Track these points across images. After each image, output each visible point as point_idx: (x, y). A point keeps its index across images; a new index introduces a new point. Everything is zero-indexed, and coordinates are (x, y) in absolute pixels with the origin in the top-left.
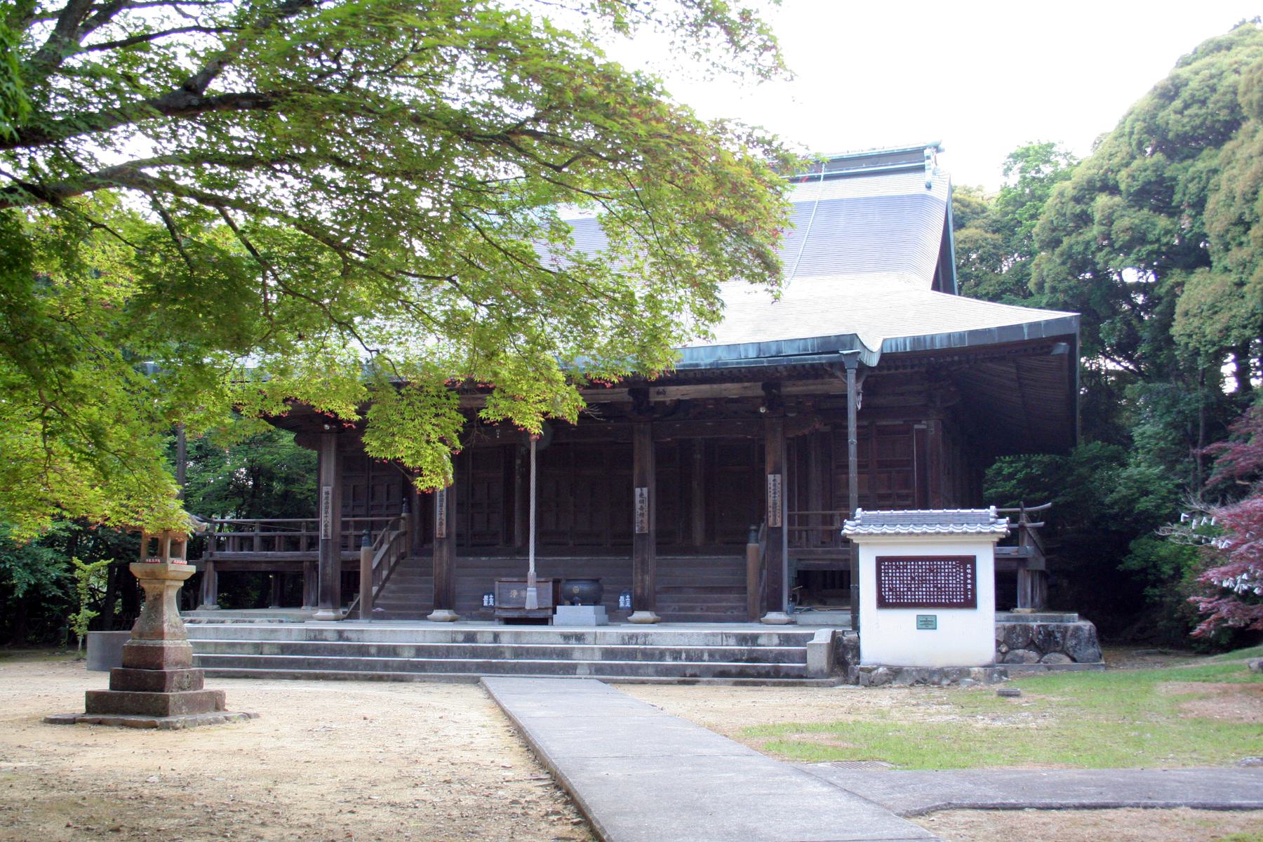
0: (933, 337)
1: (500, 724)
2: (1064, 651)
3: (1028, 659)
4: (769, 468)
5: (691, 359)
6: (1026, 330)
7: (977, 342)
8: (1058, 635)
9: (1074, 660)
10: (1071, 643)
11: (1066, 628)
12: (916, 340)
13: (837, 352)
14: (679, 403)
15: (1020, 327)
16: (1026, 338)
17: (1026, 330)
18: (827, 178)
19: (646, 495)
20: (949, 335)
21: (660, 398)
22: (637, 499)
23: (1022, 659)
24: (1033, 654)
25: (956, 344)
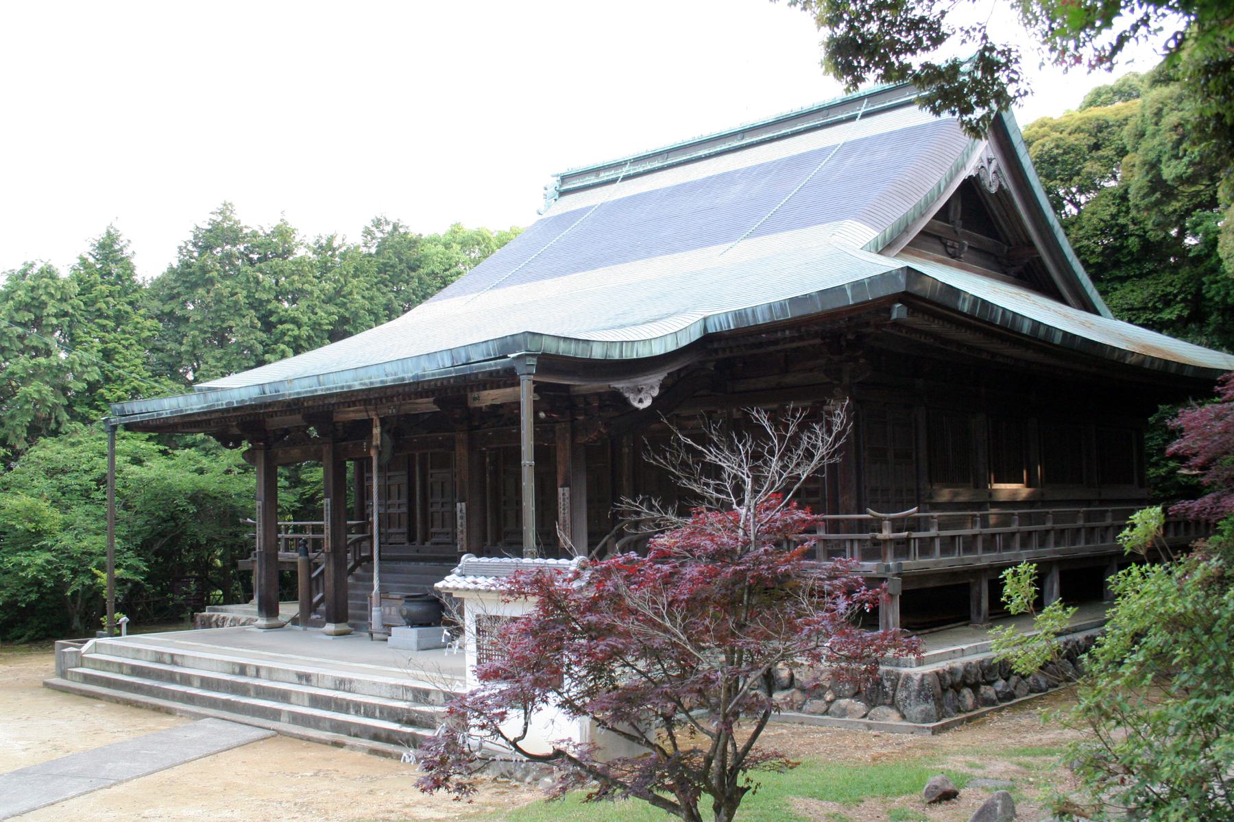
0: (754, 310)
1: (238, 754)
2: (893, 705)
3: (852, 713)
4: (560, 482)
5: (404, 372)
6: (849, 293)
7: (799, 312)
8: (887, 684)
9: (904, 717)
10: (901, 695)
11: (898, 675)
12: (738, 315)
13: (505, 357)
14: (494, 407)
15: (841, 289)
16: (851, 302)
17: (849, 293)
18: (865, 115)
19: (567, 495)
20: (770, 306)
21: (477, 404)
22: (560, 495)
23: (844, 712)
24: (860, 706)
25: (779, 317)
